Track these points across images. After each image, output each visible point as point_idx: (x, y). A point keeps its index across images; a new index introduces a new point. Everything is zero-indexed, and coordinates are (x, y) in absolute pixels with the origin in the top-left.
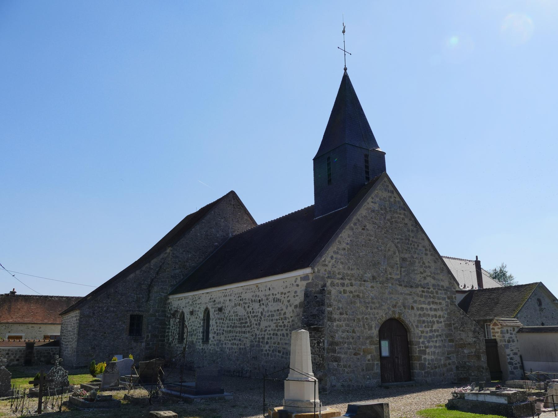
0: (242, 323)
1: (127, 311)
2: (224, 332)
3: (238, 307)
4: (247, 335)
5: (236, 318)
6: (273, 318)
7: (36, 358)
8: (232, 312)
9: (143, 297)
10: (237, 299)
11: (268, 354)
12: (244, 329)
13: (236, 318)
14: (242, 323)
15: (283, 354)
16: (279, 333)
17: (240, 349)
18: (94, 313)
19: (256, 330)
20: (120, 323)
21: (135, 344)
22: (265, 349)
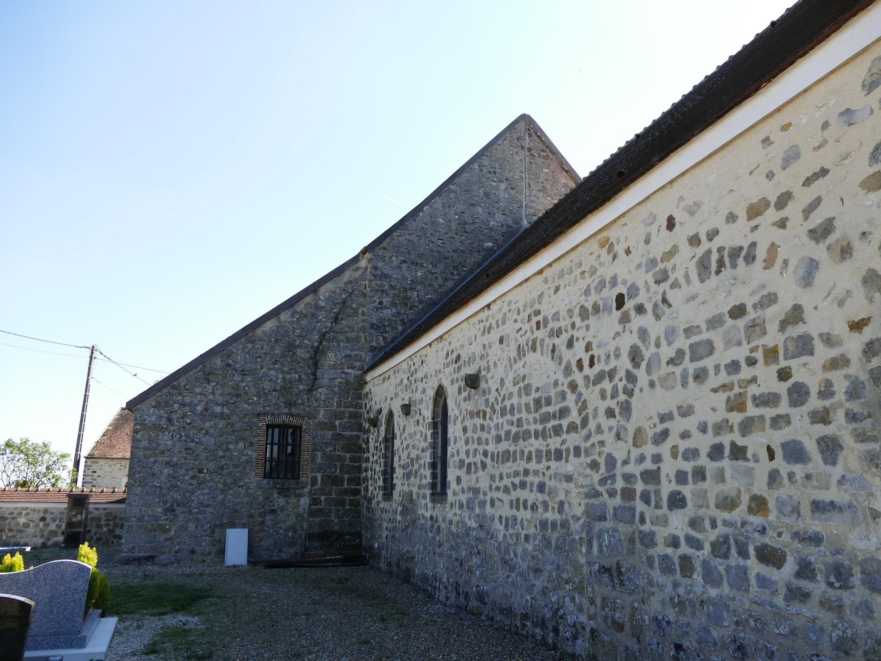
0: (546, 418)
1: (259, 415)
2: (488, 461)
3: (531, 357)
4: (571, 466)
5: (525, 399)
6: (708, 363)
7: (105, 529)
8: (509, 383)
9: (300, 380)
10: (526, 327)
11: (686, 561)
12: (554, 443)
13: (525, 399)
14: (546, 418)
15: (805, 570)
16: (755, 443)
17: (544, 524)
18: (170, 420)
19: (608, 437)
20: (241, 445)
21: (282, 501)
22: (662, 533)
